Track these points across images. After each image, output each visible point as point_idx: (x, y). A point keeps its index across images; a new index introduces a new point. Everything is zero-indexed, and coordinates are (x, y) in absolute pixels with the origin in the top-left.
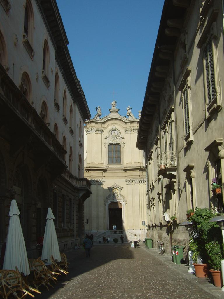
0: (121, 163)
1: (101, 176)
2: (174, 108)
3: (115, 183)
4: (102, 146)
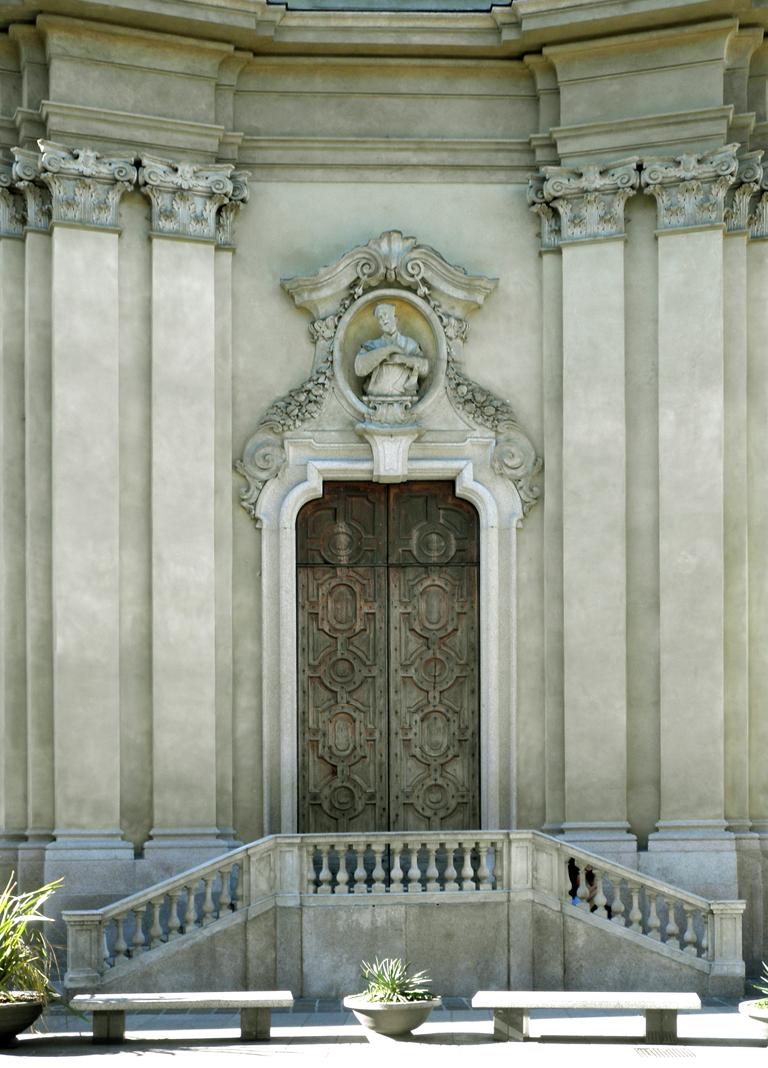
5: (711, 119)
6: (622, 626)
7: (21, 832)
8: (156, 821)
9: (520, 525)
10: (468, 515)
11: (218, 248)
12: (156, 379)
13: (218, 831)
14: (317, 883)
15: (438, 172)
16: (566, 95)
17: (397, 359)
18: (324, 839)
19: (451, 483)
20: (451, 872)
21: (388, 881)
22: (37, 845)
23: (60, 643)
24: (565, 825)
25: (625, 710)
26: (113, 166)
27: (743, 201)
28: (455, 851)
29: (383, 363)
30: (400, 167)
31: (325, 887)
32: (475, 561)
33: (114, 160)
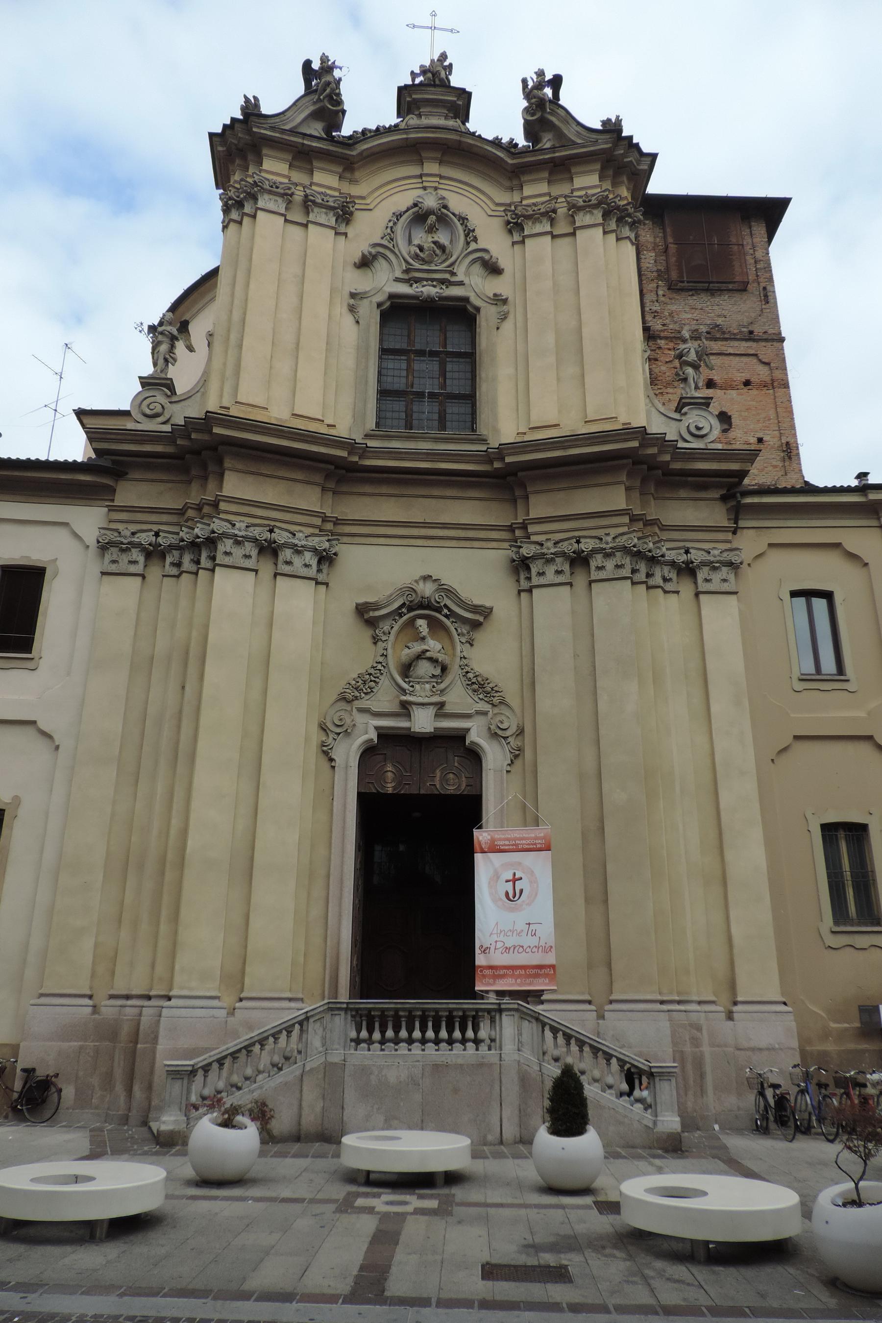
9: (509, 768)
17: (428, 654)
19: (462, 738)
28: (460, 1017)
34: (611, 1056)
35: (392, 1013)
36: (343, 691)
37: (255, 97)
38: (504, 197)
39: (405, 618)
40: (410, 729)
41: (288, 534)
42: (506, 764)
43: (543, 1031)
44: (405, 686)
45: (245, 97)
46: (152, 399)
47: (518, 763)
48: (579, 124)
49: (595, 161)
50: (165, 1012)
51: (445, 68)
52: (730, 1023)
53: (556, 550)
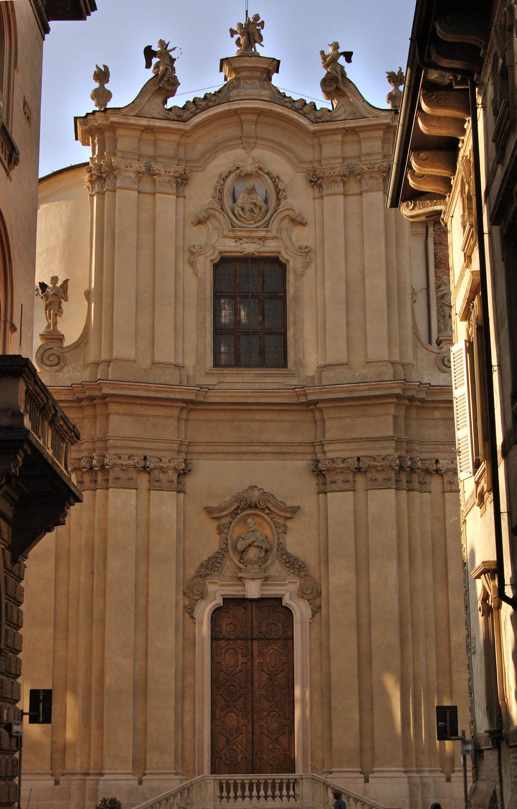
0: (285, 365)
1: (172, 442)
2: (457, 735)
3: (249, 483)
4: (181, 265)
5: (387, 440)
6: (356, 672)
7: (87, 771)
8: (148, 766)
9: (311, 621)
10: (288, 612)
11: (178, 492)
12: (151, 555)
13: (175, 771)
14: (221, 798)
15: (274, 455)
16: (328, 423)
17: (256, 544)
18: (224, 777)
19: (280, 599)
20: (277, 793)
21: (258, 797)
22: (95, 778)
23: (108, 680)
24: (333, 770)
25: (358, 712)
26: (135, 461)
27: (404, 477)
28: (279, 783)
29: (250, 546)
30: (256, 453)
31: (225, 800)
32: (291, 637)
33: (135, 458)
34: (350, 797)
35: (256, 781)
36: (198, 570)
37: (105, 67)
38: (308, 154)
39: (239, 516)
40: (245, 595)
41: (156, 460)
42: (309, 618)
43: (327, 790)
44: (241, 566)
45: (97, 66)
46: (51, 352)
47: (318, 615)
48: (364, 101)
49: (379, 129)
50: (101, 783)
51: (259, 25)
52: (449, 784)
53: (344, 465)
